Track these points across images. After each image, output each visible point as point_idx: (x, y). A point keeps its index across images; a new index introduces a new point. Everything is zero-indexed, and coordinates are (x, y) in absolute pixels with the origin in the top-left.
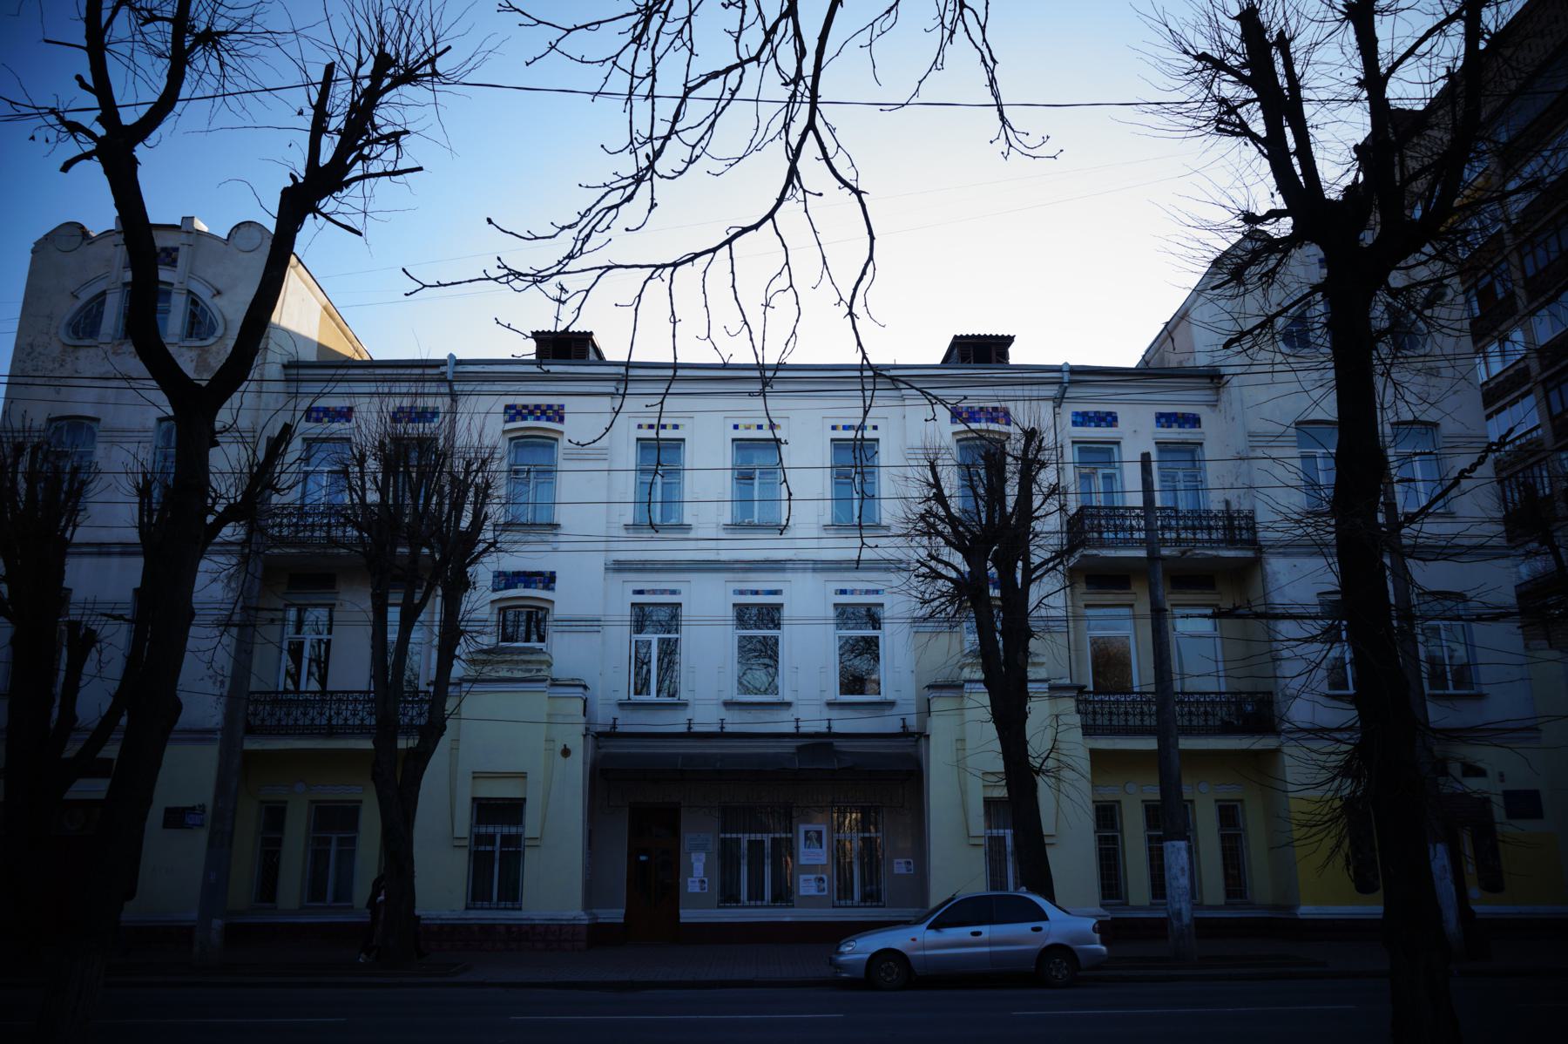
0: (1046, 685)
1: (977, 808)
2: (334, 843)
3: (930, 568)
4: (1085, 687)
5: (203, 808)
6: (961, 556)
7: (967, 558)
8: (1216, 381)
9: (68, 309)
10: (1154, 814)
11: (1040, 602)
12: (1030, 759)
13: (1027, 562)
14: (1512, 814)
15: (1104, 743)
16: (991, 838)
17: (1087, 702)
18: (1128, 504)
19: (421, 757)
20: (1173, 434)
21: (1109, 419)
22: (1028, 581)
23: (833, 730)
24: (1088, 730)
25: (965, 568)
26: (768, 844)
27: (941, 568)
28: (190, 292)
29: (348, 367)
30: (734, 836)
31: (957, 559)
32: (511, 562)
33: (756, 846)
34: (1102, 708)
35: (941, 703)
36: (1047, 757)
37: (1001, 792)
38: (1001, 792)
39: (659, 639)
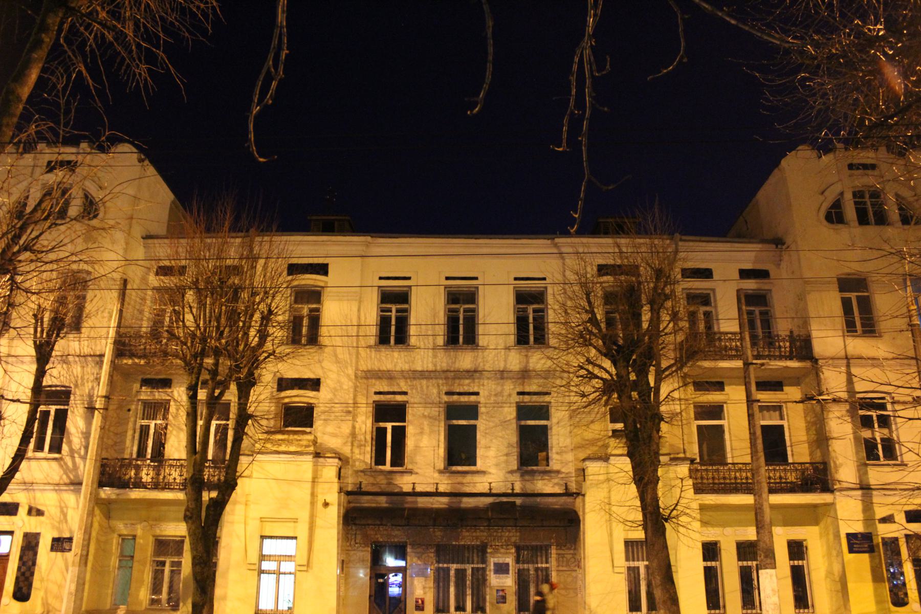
1: (620, 548)
2: (167, 565)
3: (587, 370)
4: (695, 459)
5: (548, 465)
6: (610, 362)
7: (615, 363)
8: (779, 246)
10: (745, 550)
11: (669, 395)
12: (661, 510)
13: (658, 365)
15: (711, 499)
16: (629, 568)
17: (697, 470)
18: (722, 330)
19: (218, 507)
20: (751, 285)
21: (706, 274)
22: (658, 381)
23: (439, 491)
24: (698, 490)
25: (613, 371)
26: (469, 572)
27: (596, 371)
28: (84, 190)
29: (463, 595)
30: (445, 565)
31: (607, 364)
32: (292, 369)
33: (460, 574)
34: (707, 475)
35: (593, 468)
36: (674, 509)
37: (639, 534)
38: (639, 534)
39: (393, 427)
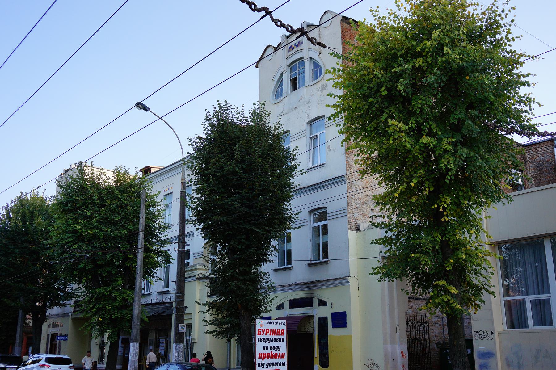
0: (195, 278)
9: (272, 86)
14: (334, 326)
28: (311, 58)
